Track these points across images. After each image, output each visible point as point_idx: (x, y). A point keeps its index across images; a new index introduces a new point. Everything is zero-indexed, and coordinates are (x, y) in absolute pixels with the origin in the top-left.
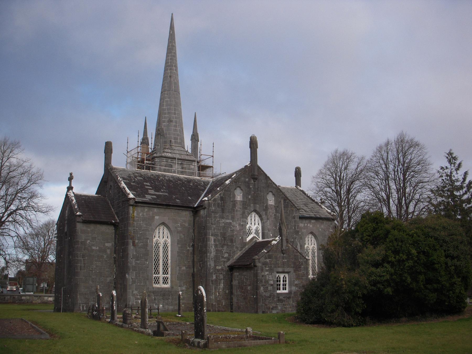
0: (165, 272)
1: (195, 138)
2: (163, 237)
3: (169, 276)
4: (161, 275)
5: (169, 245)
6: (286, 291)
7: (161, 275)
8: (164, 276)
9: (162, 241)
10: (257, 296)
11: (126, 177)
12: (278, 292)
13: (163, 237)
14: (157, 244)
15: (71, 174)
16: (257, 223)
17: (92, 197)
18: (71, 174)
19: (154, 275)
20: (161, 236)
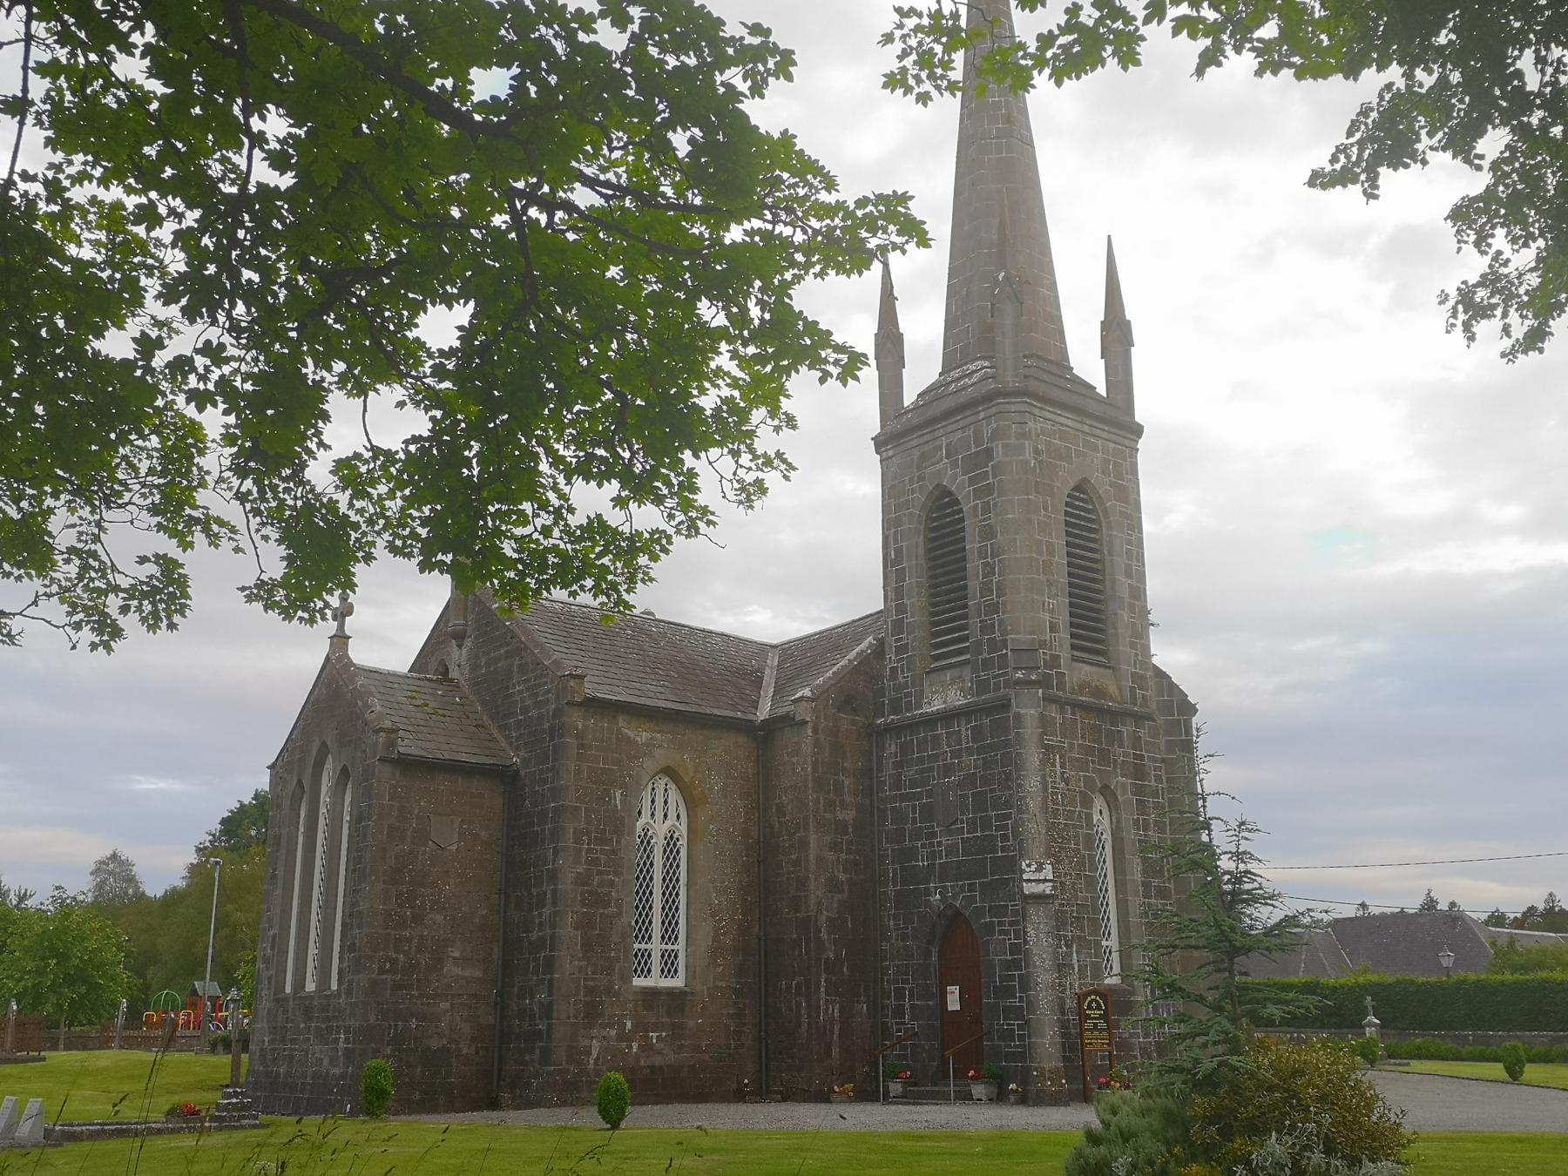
0: (669, 935)
1: (1116, 335)
2: (666, 816)
3: (680, 946)
4: (656, 946)
5: (683, 842)
6: (678, 982)
7: (656, 946)
8: (664, 947)
9: (661, 830)
10: (550, 994)
11: (1533, 264)
12: (638, 982)
13: (666, 816)
14: (646, 840)
15: (1200, 72)
16: (672, 814)
18: (1200, 72)
19: (636, 946)
20: (659, 814)
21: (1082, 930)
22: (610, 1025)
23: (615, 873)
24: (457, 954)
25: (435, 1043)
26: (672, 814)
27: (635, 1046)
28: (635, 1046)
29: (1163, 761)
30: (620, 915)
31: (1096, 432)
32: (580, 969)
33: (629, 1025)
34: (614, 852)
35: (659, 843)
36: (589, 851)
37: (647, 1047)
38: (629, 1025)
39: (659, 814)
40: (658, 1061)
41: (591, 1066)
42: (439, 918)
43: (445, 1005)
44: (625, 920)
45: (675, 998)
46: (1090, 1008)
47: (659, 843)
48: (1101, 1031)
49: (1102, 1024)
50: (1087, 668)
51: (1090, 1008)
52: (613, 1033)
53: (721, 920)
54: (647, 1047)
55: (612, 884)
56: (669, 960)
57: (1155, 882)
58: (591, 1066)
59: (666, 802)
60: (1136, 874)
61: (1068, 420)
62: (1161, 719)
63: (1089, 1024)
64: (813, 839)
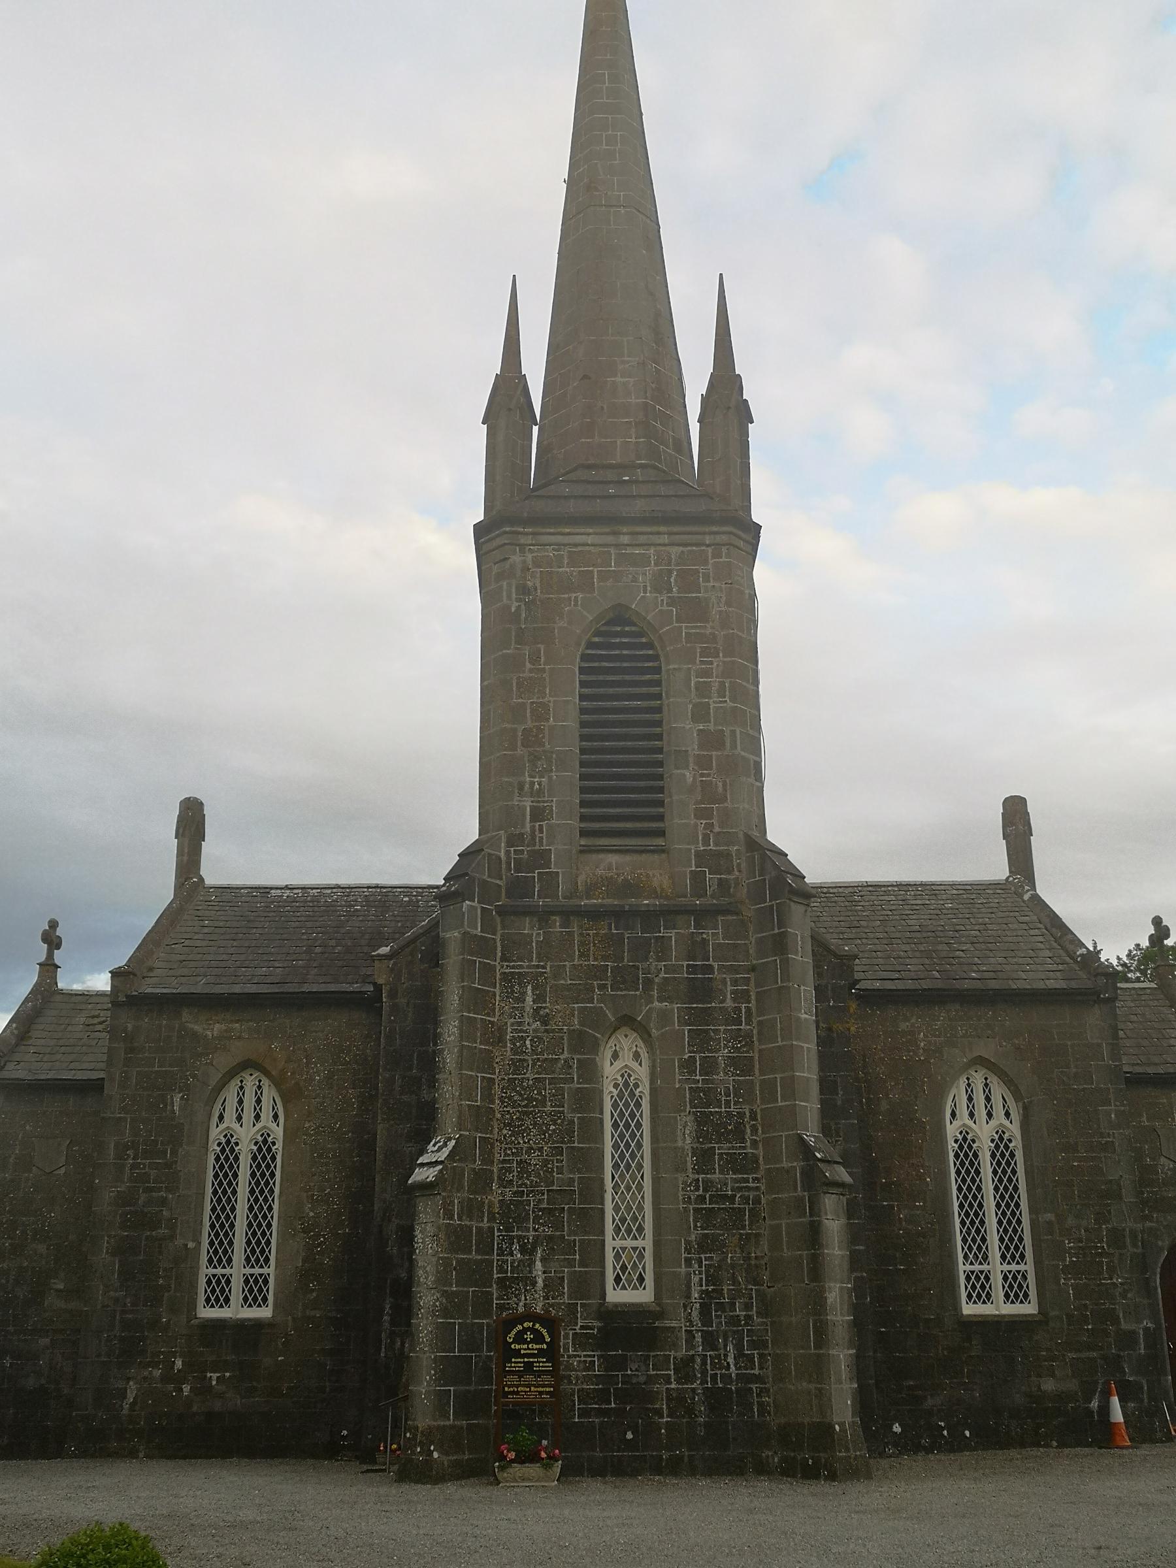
3: (1028, 1267)
5: (1017, 1144)
9: (246, 1136)
14: (966, 1143)
16: (999, 1111)
17: (101, 994)
20: (981, 1113)
21: (558, 1226)
22: (155, 1365)
23: (168, 1190)
24: (61, 1286)
25: (31, 1383)
26: (999, 1111)
27: (186, 1389)
28: (186, 1389)
29: (753, 969)
30: (172, 1237)
31: (642, 539)
32: (117, 1300)
33: (179, 1364)
34: (168, 1166)
35: (245, 1150)
36: (133, 1167)
37: (202, 1389)
38: (179, 1364)
39: (981, 1113)
40: (218, 1406)
41: (125, 1412)
42: (42, 1248)
43: (45, 1341)
44: (179, 1242)
45: (247, 1334)
46: (519, 1339)
47: (245, 1150)
48: (540, 1373)
49: (542, 1364)
50: (613, 859)
51: (519, 1339)
52: (157, 1373)
53: (318, 1236)
54: (202, 1389)
55: (163, 1202)
56: (255, 1292)
57: (721, 1148)
58: (125, 1412)
59: (259, 1101)
60: (685, 1139)
61: (589, 537)
62: (749, 910)
63: (516, 1364)
64: (381, 1130)
